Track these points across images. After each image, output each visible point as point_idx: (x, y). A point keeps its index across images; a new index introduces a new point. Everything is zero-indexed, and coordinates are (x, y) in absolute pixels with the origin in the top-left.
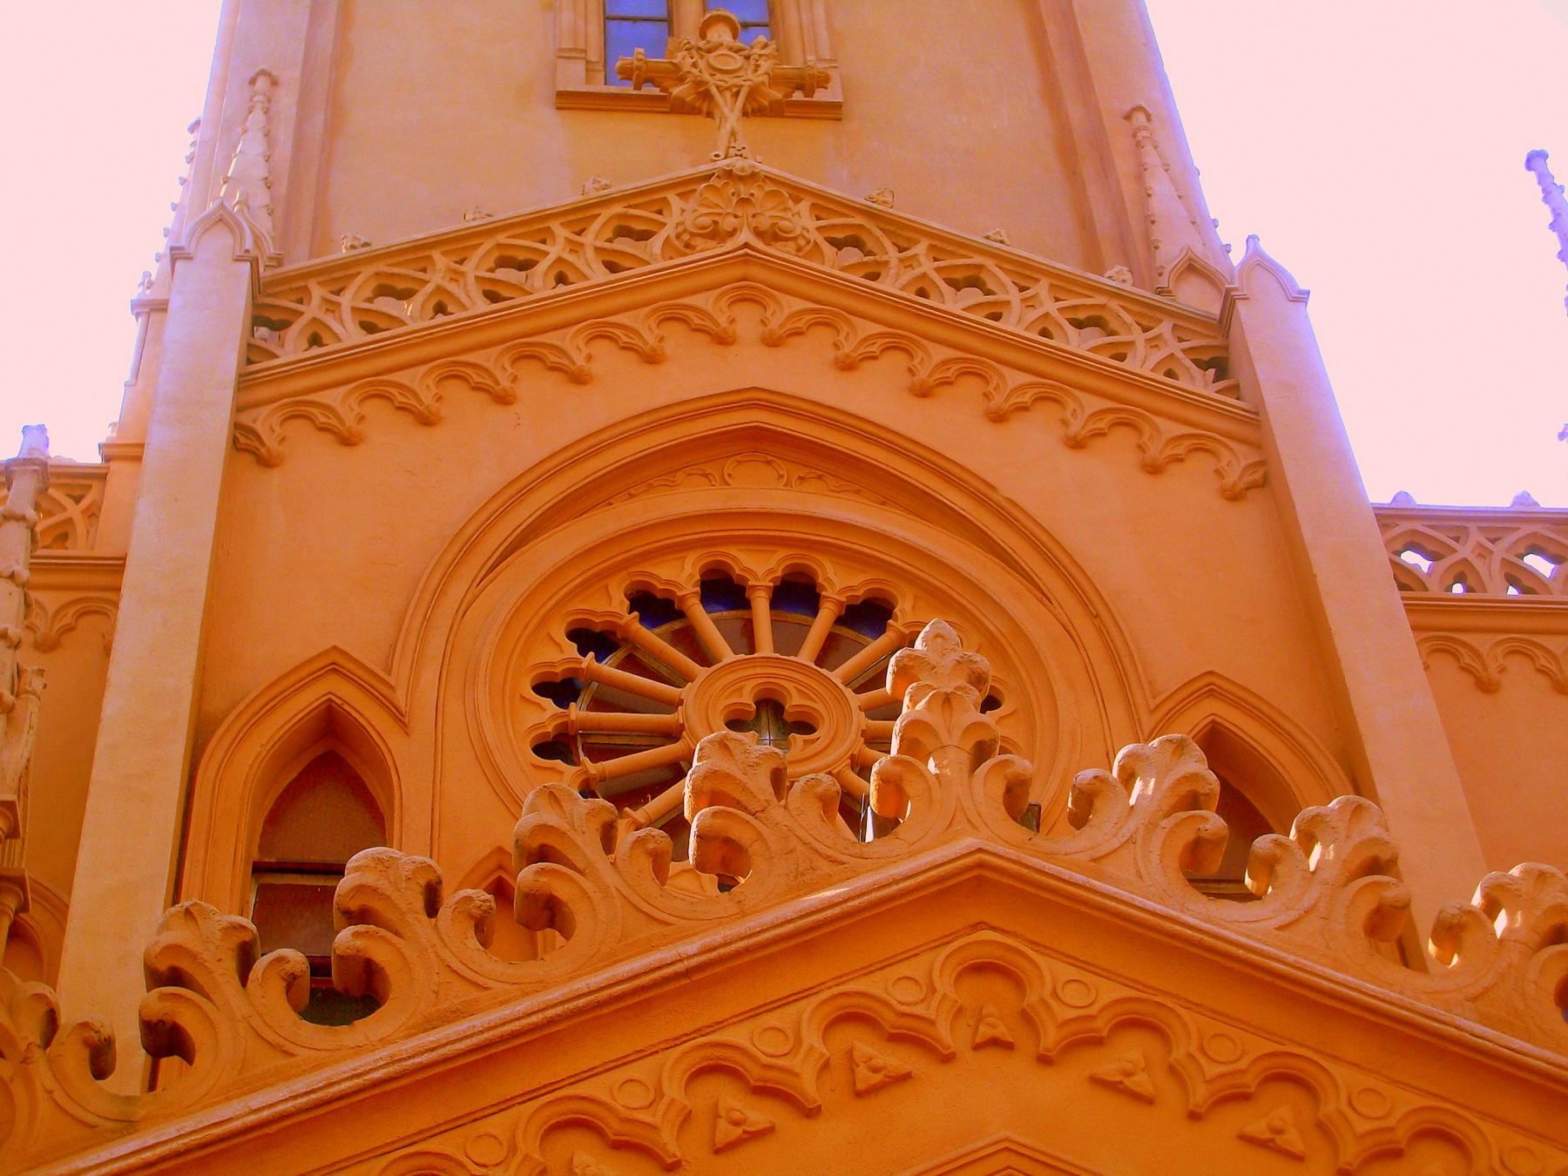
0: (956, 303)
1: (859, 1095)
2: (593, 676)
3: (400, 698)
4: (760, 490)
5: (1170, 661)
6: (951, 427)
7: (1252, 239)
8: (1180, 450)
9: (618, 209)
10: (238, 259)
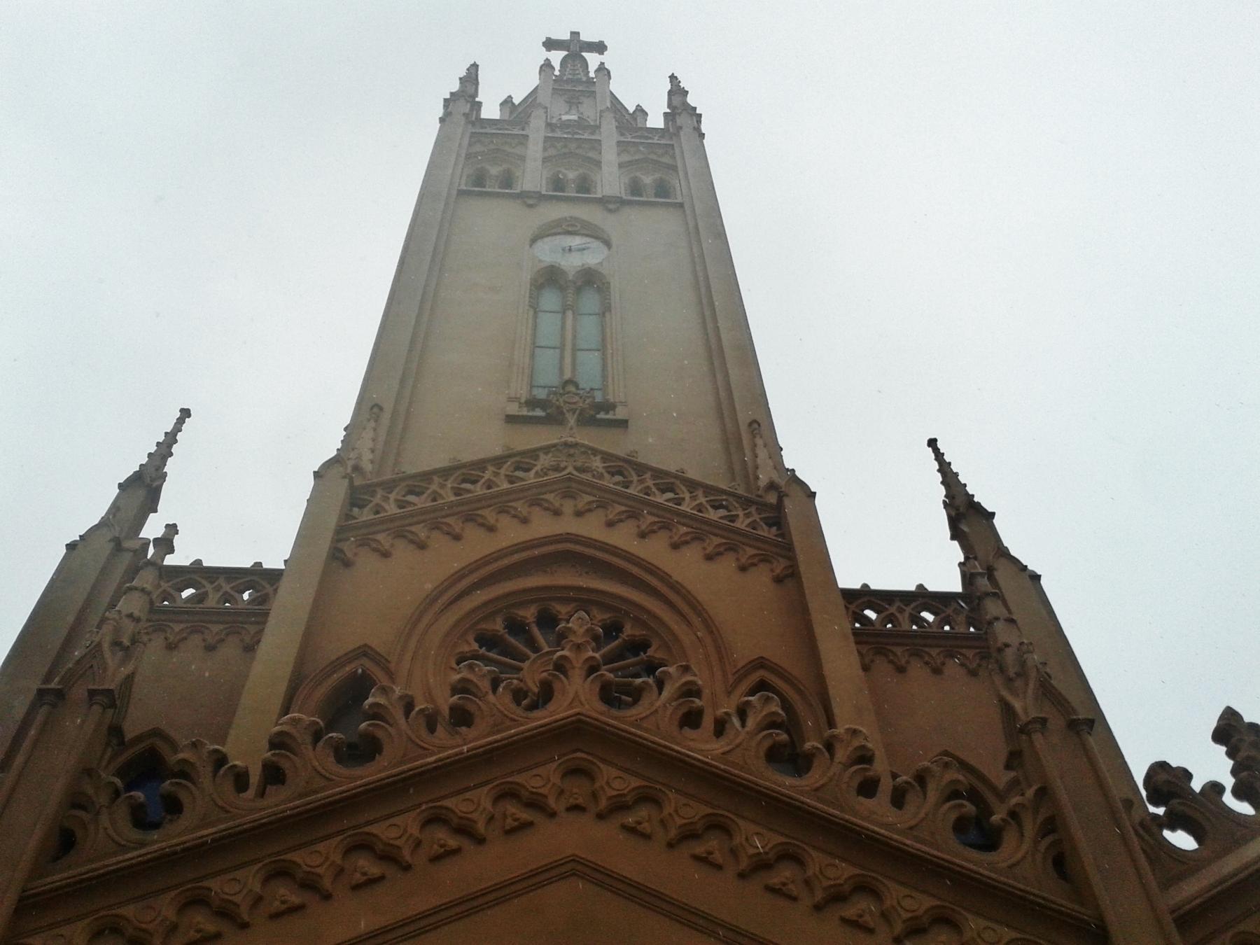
0: (660, 498)
3: (392, 666)
5: (744, 649)
8: (755, 561)
9: (517, 459)
10: (344, 477)
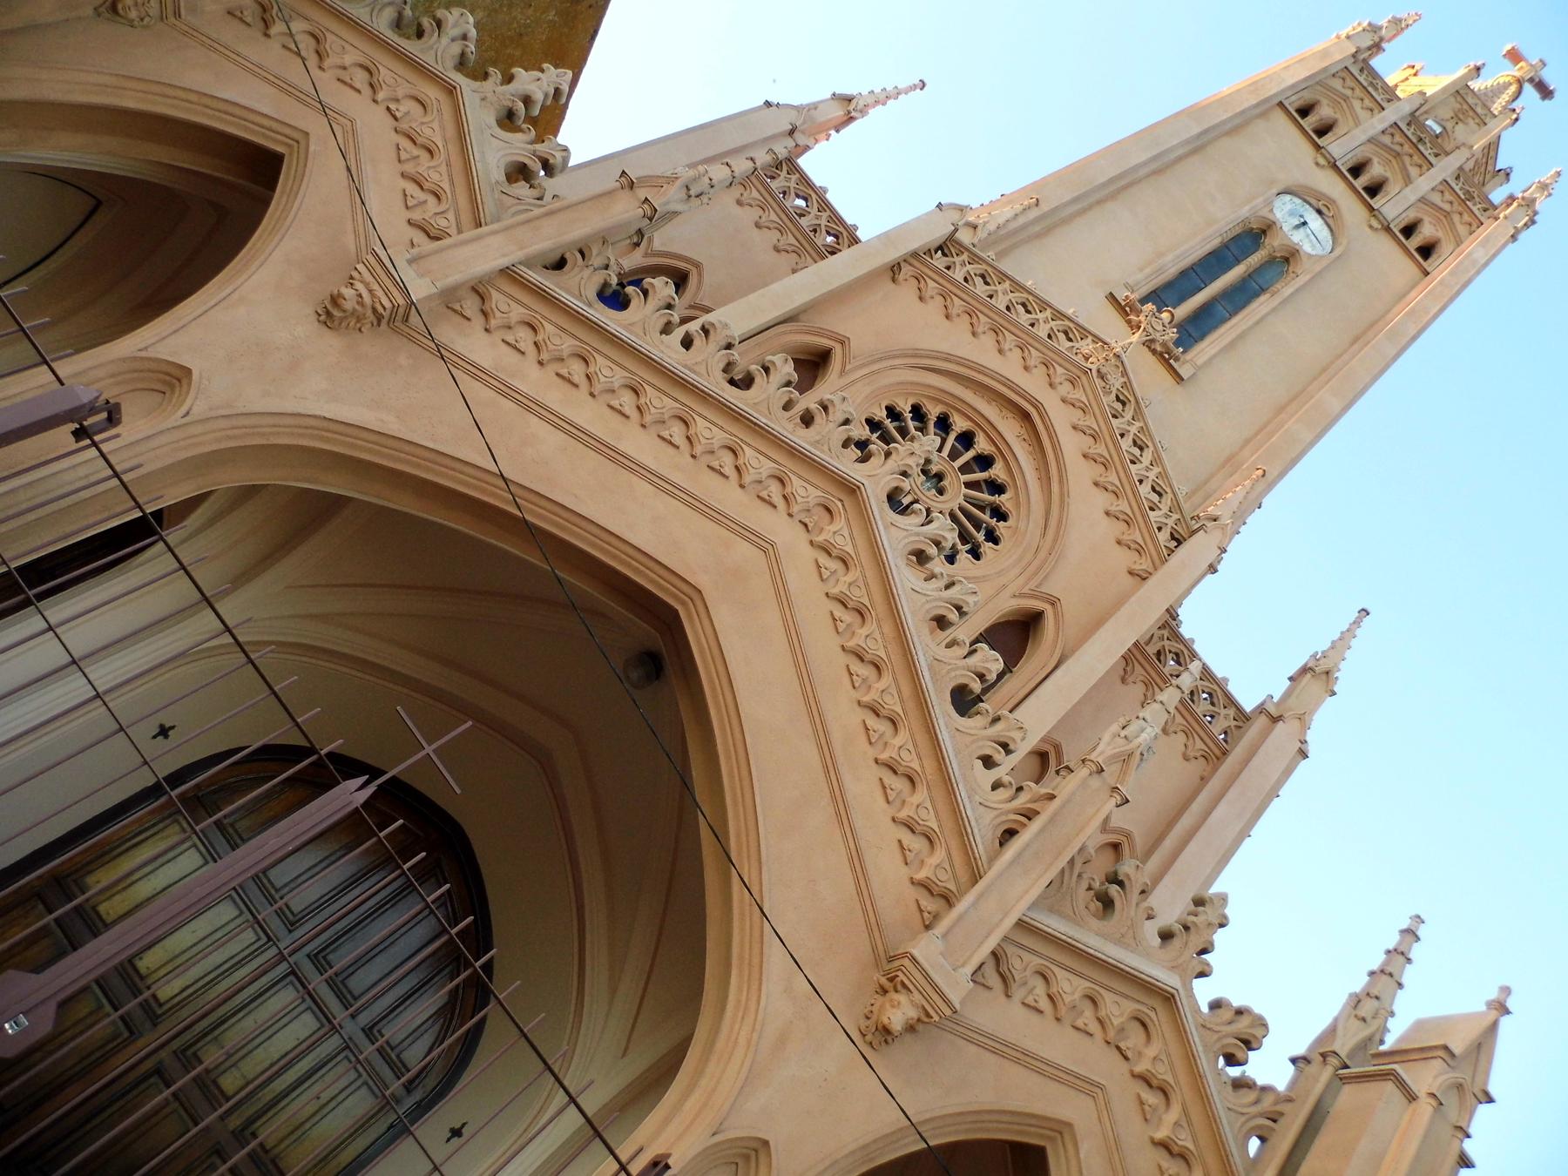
2: (904, 420)
4: (1010, 429)
6: (1080, 474)
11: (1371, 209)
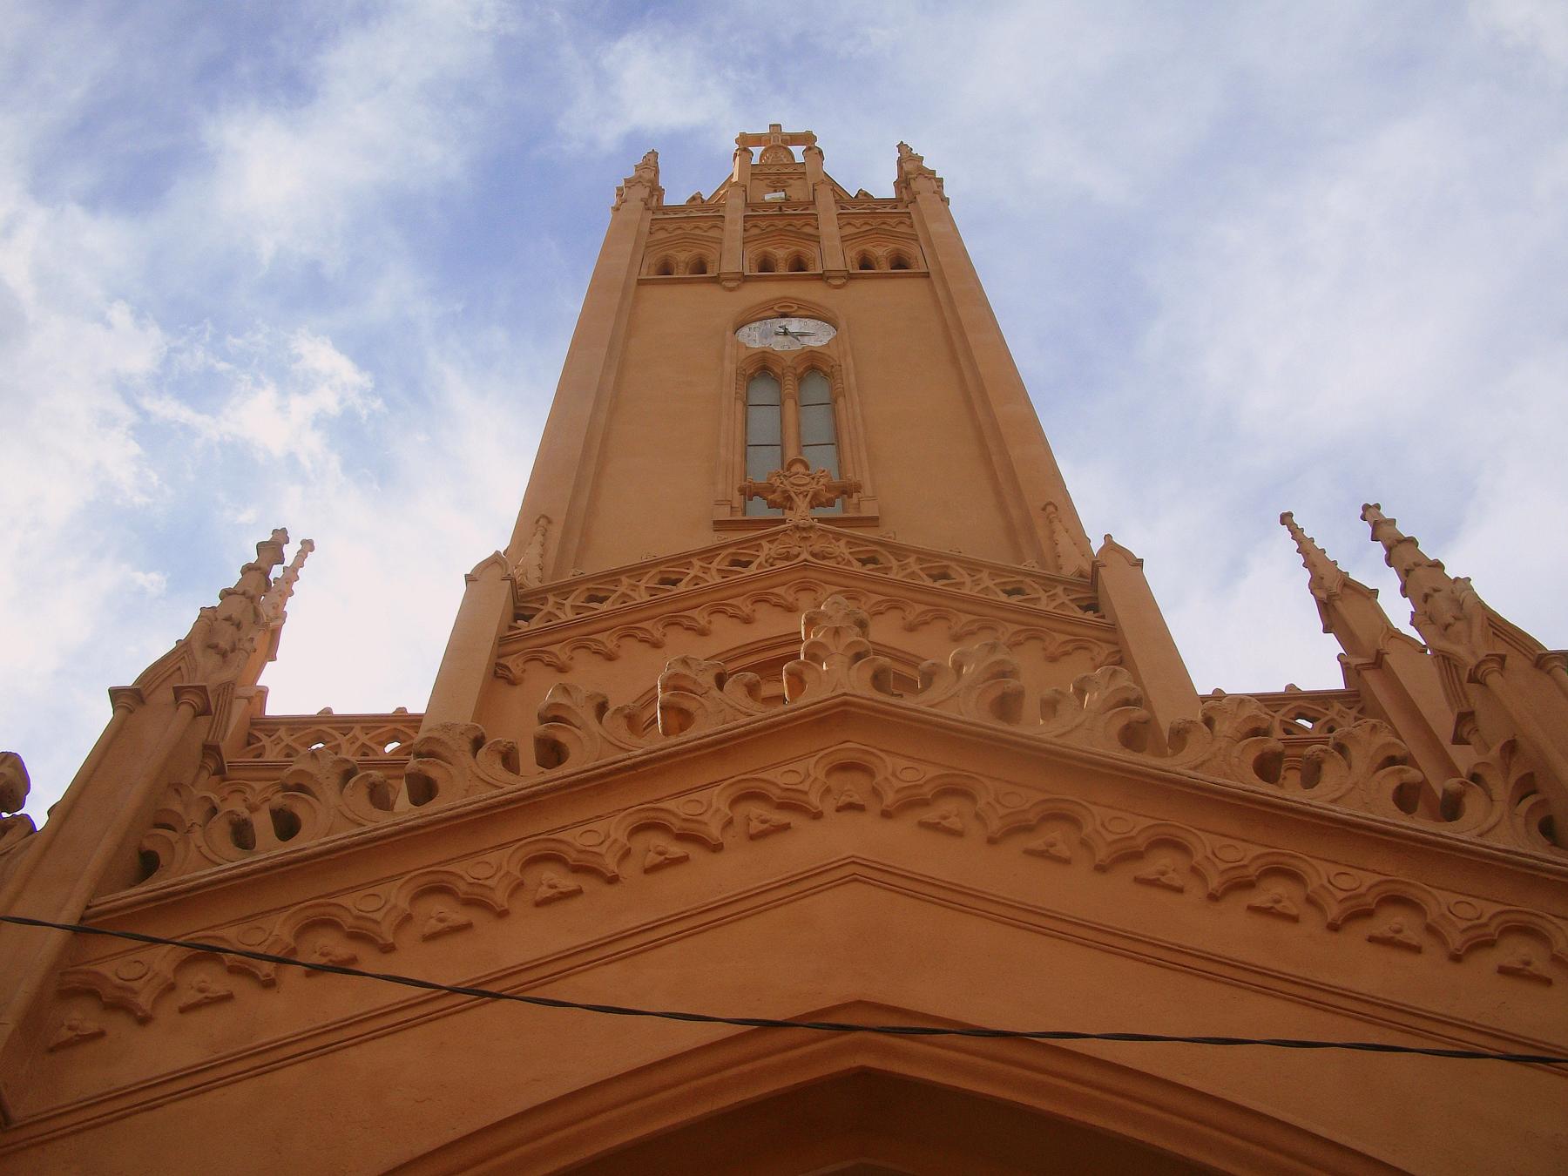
1: (752, 838)
7: (1108, 537)
8: (1069, 648)
11: (820, 277)
